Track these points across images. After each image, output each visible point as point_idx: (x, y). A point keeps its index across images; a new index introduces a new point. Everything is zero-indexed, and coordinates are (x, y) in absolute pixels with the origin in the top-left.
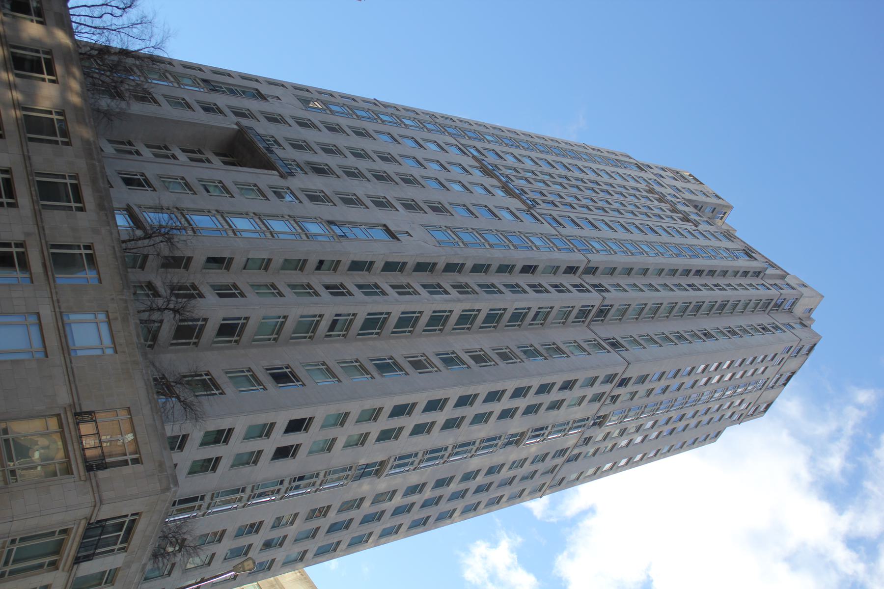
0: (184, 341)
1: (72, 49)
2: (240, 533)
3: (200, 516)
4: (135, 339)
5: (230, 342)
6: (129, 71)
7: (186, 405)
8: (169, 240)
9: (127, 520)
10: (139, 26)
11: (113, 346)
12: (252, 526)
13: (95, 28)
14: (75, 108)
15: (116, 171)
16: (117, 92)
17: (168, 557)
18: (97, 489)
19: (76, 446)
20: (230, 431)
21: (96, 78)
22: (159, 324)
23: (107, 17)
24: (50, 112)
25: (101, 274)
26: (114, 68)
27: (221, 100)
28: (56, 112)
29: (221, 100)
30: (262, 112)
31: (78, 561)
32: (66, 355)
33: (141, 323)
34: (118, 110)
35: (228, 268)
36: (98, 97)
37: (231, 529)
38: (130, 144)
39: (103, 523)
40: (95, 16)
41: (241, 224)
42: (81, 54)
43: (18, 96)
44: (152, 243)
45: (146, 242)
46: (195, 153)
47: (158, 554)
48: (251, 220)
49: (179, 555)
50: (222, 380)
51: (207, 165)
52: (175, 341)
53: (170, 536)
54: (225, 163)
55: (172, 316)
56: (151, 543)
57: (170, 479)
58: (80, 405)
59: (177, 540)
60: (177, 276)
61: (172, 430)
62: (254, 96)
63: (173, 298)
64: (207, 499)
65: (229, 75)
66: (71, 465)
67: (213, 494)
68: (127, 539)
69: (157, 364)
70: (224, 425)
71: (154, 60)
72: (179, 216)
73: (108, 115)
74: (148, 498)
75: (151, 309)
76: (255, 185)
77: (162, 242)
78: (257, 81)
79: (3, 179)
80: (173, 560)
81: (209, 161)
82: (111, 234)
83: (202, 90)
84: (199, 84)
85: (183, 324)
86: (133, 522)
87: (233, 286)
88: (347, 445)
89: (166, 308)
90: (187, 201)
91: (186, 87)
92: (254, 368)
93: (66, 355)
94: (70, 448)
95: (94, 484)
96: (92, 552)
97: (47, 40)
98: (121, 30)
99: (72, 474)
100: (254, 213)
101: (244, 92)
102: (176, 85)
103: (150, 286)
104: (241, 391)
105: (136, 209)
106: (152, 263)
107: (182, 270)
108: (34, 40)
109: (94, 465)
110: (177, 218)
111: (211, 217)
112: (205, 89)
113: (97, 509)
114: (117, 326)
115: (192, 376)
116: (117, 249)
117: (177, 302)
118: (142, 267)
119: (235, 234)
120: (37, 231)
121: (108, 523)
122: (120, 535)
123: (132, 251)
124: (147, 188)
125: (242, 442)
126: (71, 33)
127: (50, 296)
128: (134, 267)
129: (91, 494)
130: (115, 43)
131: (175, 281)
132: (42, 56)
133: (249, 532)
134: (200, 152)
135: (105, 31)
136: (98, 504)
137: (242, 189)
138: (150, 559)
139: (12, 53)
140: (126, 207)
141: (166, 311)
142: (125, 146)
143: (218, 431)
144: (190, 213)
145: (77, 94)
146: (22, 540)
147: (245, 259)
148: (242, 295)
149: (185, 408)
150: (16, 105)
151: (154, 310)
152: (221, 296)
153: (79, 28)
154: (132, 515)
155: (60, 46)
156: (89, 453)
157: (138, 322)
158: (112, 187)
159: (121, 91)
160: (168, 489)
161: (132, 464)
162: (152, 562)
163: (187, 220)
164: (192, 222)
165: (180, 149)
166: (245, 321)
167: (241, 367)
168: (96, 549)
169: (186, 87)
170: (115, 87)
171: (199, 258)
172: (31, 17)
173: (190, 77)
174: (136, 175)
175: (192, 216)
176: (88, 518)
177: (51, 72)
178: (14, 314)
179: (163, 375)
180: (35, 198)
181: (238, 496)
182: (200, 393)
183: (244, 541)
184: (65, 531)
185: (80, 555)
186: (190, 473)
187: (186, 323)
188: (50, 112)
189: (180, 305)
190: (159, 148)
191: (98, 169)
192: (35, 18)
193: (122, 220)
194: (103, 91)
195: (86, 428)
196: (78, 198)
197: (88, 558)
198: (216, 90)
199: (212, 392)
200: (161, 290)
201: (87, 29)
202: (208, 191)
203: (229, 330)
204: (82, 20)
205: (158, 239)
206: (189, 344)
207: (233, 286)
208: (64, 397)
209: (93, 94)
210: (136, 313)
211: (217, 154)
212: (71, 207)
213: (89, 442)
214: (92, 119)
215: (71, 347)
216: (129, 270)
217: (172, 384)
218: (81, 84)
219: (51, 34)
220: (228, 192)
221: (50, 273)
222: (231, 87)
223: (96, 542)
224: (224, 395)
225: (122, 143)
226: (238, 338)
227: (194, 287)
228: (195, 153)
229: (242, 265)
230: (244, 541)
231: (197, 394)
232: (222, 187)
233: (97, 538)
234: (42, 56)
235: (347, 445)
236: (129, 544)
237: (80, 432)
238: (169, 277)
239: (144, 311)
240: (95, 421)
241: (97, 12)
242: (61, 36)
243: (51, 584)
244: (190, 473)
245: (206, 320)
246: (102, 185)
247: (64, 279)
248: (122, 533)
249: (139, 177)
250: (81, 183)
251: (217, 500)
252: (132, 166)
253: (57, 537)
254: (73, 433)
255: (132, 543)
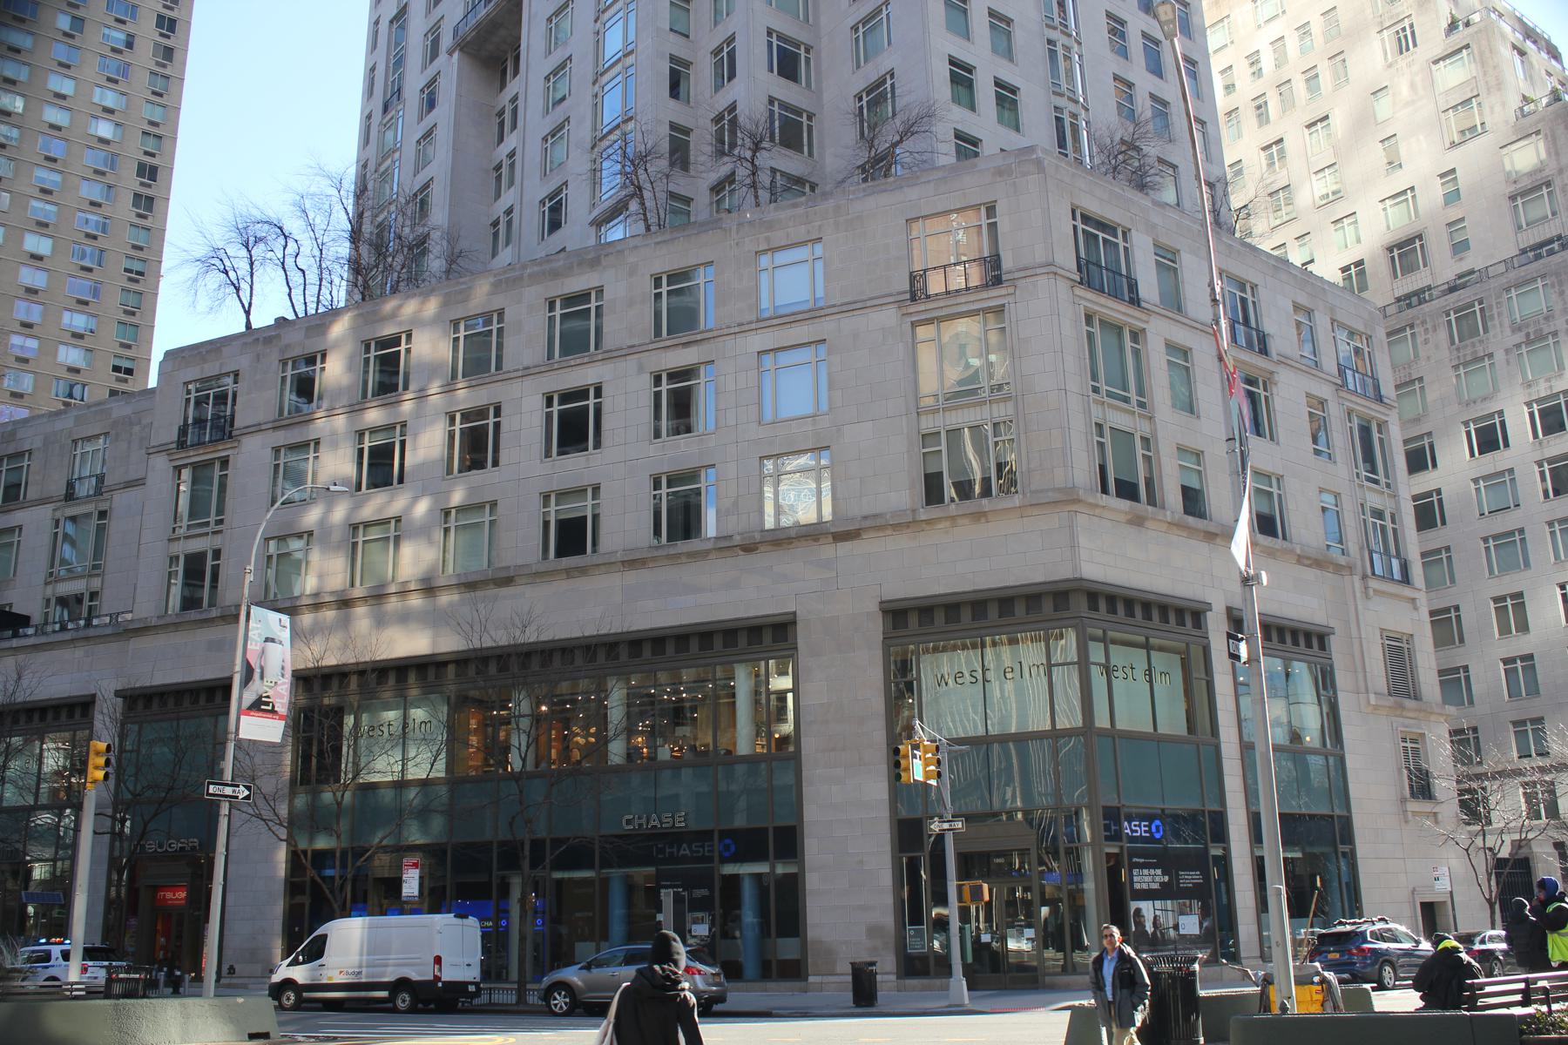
0: (805, 135)
1: (356, 312)
2: (1123, 52)
3: (1088, 116)
4: (800, 210)
5: (808, 60)
6: (382, 228)
7: (907, 132)
8: (643, 159)
9: (1081, 226)
10: (311, 216)
11: (810, 244)
12: (1112, 31)
13: (321, 280)
14: (445, 305)
15: (539, 244)
16: (418, 246)
17: (1148, 168)
18: (1029, 271)
19: (962, 299)
20: (953, 62)
21: (399, 277)
22: (778, 174)
23: (302, 262)
24: (456, 340)
25: (700, 262)
26: (379, 248)
27: (414, 81)
28: (445, 523)
29: (414, 81)
30: (428, 12)
31: (1135, 301)
32: (822, 313)
33: (776, 201)
34: (445, 243)
35: (687, 65)
36: (428, 273)
37: (1114, 64)
38: (495, 224)
39: (1083, 262)
40: (302, 281)
41: (614, 42)
42: (363, 299)
43: (434, 388)
44: (648, 186)
45: (647, 194)
46: (503, 121)
47: (1141, 183)
48: (607, 26)
49: (1146, 149)
50: (871, 73)
51: (520, 102)
52: (806, 149)
53: (1113, 162)
54: (516, 72)
55: (764, 152)
56: (1121, 192)
57: (1024, 158)
58: (900, 293)
59: (1121, 153)
60: (701, 145)
61: (946, 153)
62: (402, 28)
63: (736, 152)
64: (1062, 102)
65: (373, 69)
66: (990, 308)
67: (1054, 93)
68: (1109, 228)
69: (840, 177)
70: (944, 70)
71: (361, 192)
72: (606, 143)
73: (453, 260)
74: (1050, 194)
75: (754, 185)
76: (549, 20)
77: (646, 170)
78: (377, 23)
79: (559, 454)
80: (1152, 160)
81: (515, 99)
82: (636, 247)
83: (401, 113)
84: (392, 118)
85: (777, 135)
86: (1086, 219)
87: (716, 55)
88: (1009, 54)
89: (752, 163)
90: (580, 132)
91: (399, 139)
92: (851, 22)
93: (822, 313)
94: (964, 308)
95: (1022, 274)
96: (1124, 280)
97: (349, 348)
98: (319, 241)
99: (1003, 305)
100: (596, 21)
101: (397, 44)
102: (397, 155)
103: (717, 189)
104: (889, 43)
105: (596, 213)
106: (681, 185)
107: (692, 138)
108: (350, 368)
109: (994, 270)
110: (608, 147)
111: (603, 192)
112: (399, 108)
113: (1060, 271)
114: (779, 237)
115: (862, 122)
116: (659, 239)
117: (743, 145)
118: (687, 201)
119: (631, 52)
120: (636, 356)
121: (1083, 255)
122: (1104, 239)
123: (662, 216)
124: (563, 195)
125: (973, 43)
126: (334, 313)
127: (733, 336)
128: (688, 213)
129: (1035, 278)
130: (340, 250)
131: (708, 149)
132: (373, 354)
133: (1123, 36)
134: (501, 113)
135: (324, 265)
136: (1053, 269)
137: (556, 43)
138: (1147, 194)
139: (373, 396)
140: (594, 227)
141: (757, 163)
142: (500, 231)
143: (952, 81)
144: (599, 127)
145: (423, 303)
146: (1094, 377)
147: (672, 36)
148: (731, 40)
149: (912, 134)
150: (449, 389)
151: (754, 182)
152: (732, 76)
153: (326, 304)
154: (1074, 218)
155: (354, 329)
156: (975, 281)
157: (773, 205)
158: (564, 249)
159: (414, 239)
160: (1039, 163)
161: (995, 217)
162: (1151, 192)
163: (610, 132)
164: (614, 124)
165: (498, 145)
166: (774, 35)
167: (849, 43)
168: (1121, 275)
169: (399, 139)
170: (410, 249)
171: (674, 111)
172: (318, 371)
173: (382, 134)
174: (544, 212)
175: (605, 123)
176: (1072, 283)
177: (395, 341)
178: (760, 388)
179: (858, 167)
180: (586, 360)
181: (1060, 51)
182: (890, 108)
183: (1136, 44)
184: (1089, 319)
185: (1127, 298)
186: (1018, 130)
187: (777, 131)
188: (456, 340)
189: (747, 140)
190: (499, 178)
191: (536, 269)
192: (319, 366)
193: (616, 233)
194: (417, 266)
195: (935, 284)
196: (584, 297)
197: (1133, 286)
198: (399, 90)
199: (889, 89)
200: (725, 170)
201: (324, 291)
202: (563, 99)
203: (788, 63)
204: (311, 299)
205: (642, 176)
206: (810, 128)
207: (716, 55)
208: (888, 317)
209: (424, 281)
210: (758, 209)
211: (503, 85)
212: (597, 307)
213: (958, 282)
214: (461, 280)
215: (810, 305)
216: (692, 219)
217: (873, 154)
218: (408, 297)
219: (337, 345)
220: (562, 66)
221: (699, 337)
222: (391, 65)
223: (1110, 274)
224: (895, 71)
225: (496, 235)
226: (802, 48)
227: (718, 119)
228: (504, 122)
229: (682, 40)
230: (1136, 44)
231: (890, 114)
232: (555, 75)
233: (1104, 271)
234: (373, 354)
235: (1009, 54)
236: (1119, 225)
237: (941, 294)
238: (703, 158)
239: (756, 197)
240: (925, 271)
241: (296, 278)
242: (339, 329)
243: (1165, 339)
244: (1018, 130)
245: (771, 101)
246: (561, 263)
247: (709, 317)
248: (1101, 235)
249: (546, 208)
250: (560, 293)
251: (1064, 86)
252: (530, 220)
253: (1096, 330)
254: (941, 304)
255: (1119, 221)
